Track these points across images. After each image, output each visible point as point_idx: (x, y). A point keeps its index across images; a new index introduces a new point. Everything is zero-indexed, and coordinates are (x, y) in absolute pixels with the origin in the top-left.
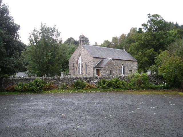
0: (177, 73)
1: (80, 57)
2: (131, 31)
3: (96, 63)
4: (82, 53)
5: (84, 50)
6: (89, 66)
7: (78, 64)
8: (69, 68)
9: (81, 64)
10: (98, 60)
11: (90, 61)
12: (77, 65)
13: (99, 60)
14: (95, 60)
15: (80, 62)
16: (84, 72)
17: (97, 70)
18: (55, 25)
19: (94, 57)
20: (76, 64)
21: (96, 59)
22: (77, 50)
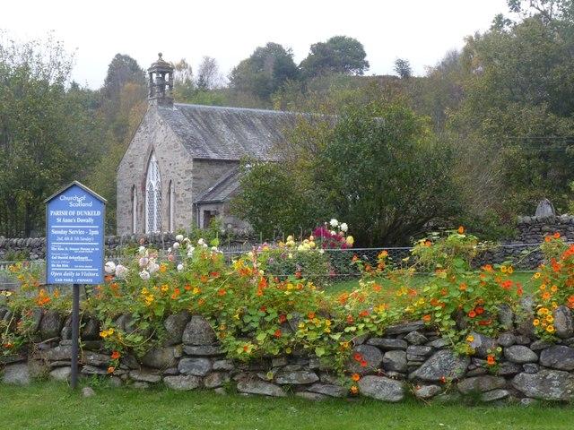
0: (532, 116)
1: (154, 159)
2: (333, 41)
3: (205, 182)
4: (158, 141)
5: (163, 128)
6: (180, 198)
7: (148, 189)
8: (119, 206)
9: (155, 187)
10: (217, 170)
11: (183, 174)
12: (144, 196)
13: (224, 172)
14: (202, 174)
15: (153, 181)
16: (165, 223)
17: (205, 211)
18: (160, 55)
19: (195, 160)
20: (140, 191)
21: (206, 166)
22: (143, 128)
